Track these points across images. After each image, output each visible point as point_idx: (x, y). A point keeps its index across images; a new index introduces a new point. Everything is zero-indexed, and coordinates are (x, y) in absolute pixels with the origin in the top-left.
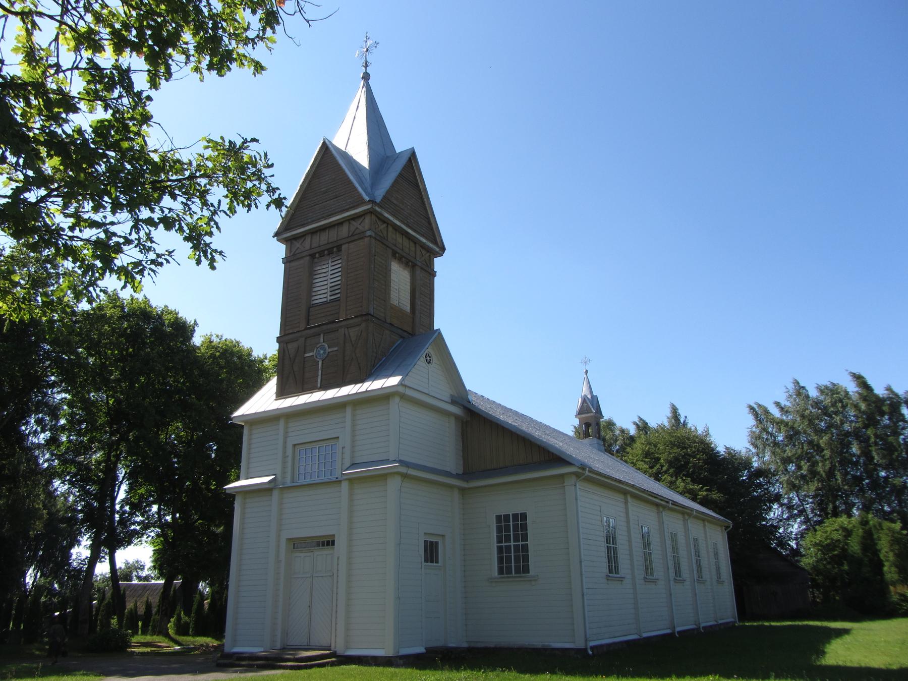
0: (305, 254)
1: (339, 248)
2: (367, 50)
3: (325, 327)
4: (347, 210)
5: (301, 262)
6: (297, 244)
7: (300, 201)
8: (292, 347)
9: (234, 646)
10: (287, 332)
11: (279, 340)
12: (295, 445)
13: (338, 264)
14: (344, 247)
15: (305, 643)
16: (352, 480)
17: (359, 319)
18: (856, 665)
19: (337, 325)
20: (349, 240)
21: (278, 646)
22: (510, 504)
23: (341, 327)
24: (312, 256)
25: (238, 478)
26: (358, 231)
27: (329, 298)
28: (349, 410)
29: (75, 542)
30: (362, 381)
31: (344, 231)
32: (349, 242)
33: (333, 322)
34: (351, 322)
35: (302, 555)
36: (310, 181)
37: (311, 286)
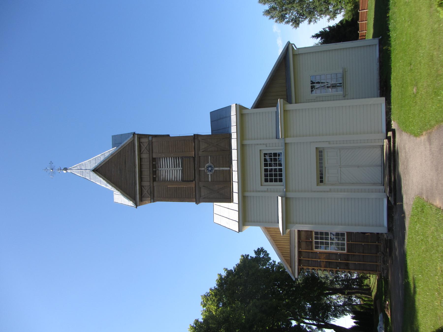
0: (152, 185)
1: (154, 159)
2: (52, 169)
3: (196, 166)
4: (134, 151)
5: (155, 188)
6: (145, 192)
7: (121, 189)
8: (204, 192)
9: (383, 226)
10: (194, 196)
11: (197, 203)
12: (261, 185)
13: (163, 162)
14: (154, 157)
15: (380, 168)
16: (286, 136)
17: (196, 140)
18: (391, 27)
19: (196, 156)
20: (151, 152)
21: (382, 187)
22: (306, 86)
23: (198, 154)
24: (154, 180)
25: (279, 229)
26: (148, 148)
27: (180, 168)
28: (247, 194)
29: (310, 304)
30: (230, 135)
31: (145, 156)
32: (152, 153)
33: (194, 158)
34: (196, 146)
35: (327, 175)
36: (112, 182)
37: (171, 182)
